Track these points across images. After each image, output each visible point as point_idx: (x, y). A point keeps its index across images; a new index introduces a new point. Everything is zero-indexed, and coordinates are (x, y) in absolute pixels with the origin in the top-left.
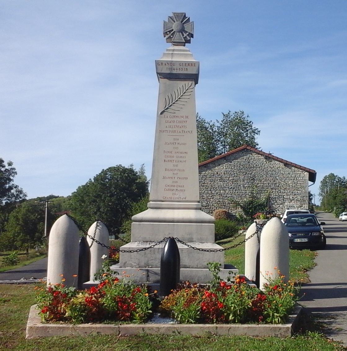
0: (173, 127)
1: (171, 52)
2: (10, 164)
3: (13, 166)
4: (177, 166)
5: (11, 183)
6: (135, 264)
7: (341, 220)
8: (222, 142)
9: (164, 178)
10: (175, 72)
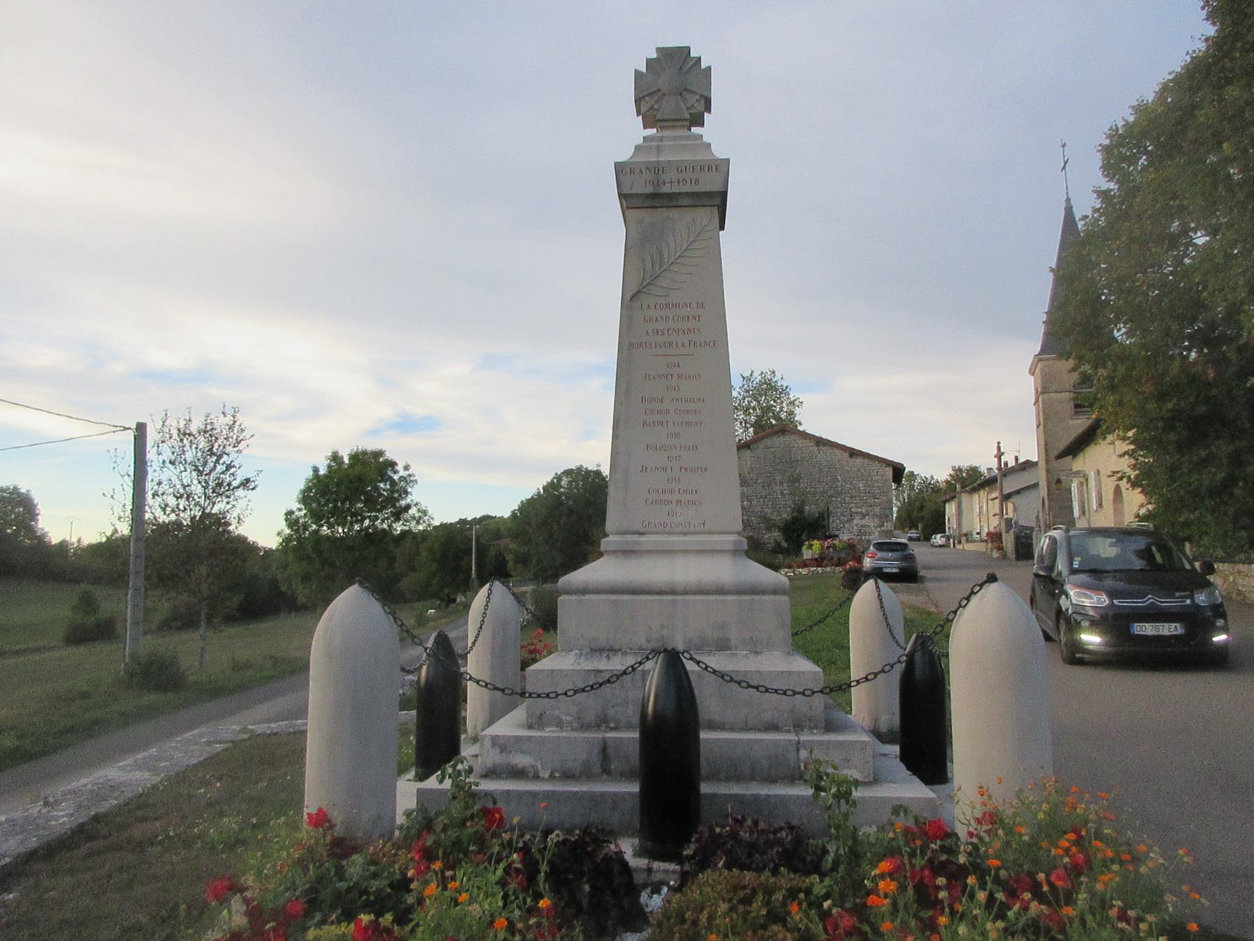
0: (666, 331)
1: (655, 143)
2: (406, 468)
3: (410, 472)
4: (677, 435)
5: (409, 500)
6: (569, 718)
7: (932, 546)
8: (741, 423)
9: (644, 469)
10: (666, 189)
